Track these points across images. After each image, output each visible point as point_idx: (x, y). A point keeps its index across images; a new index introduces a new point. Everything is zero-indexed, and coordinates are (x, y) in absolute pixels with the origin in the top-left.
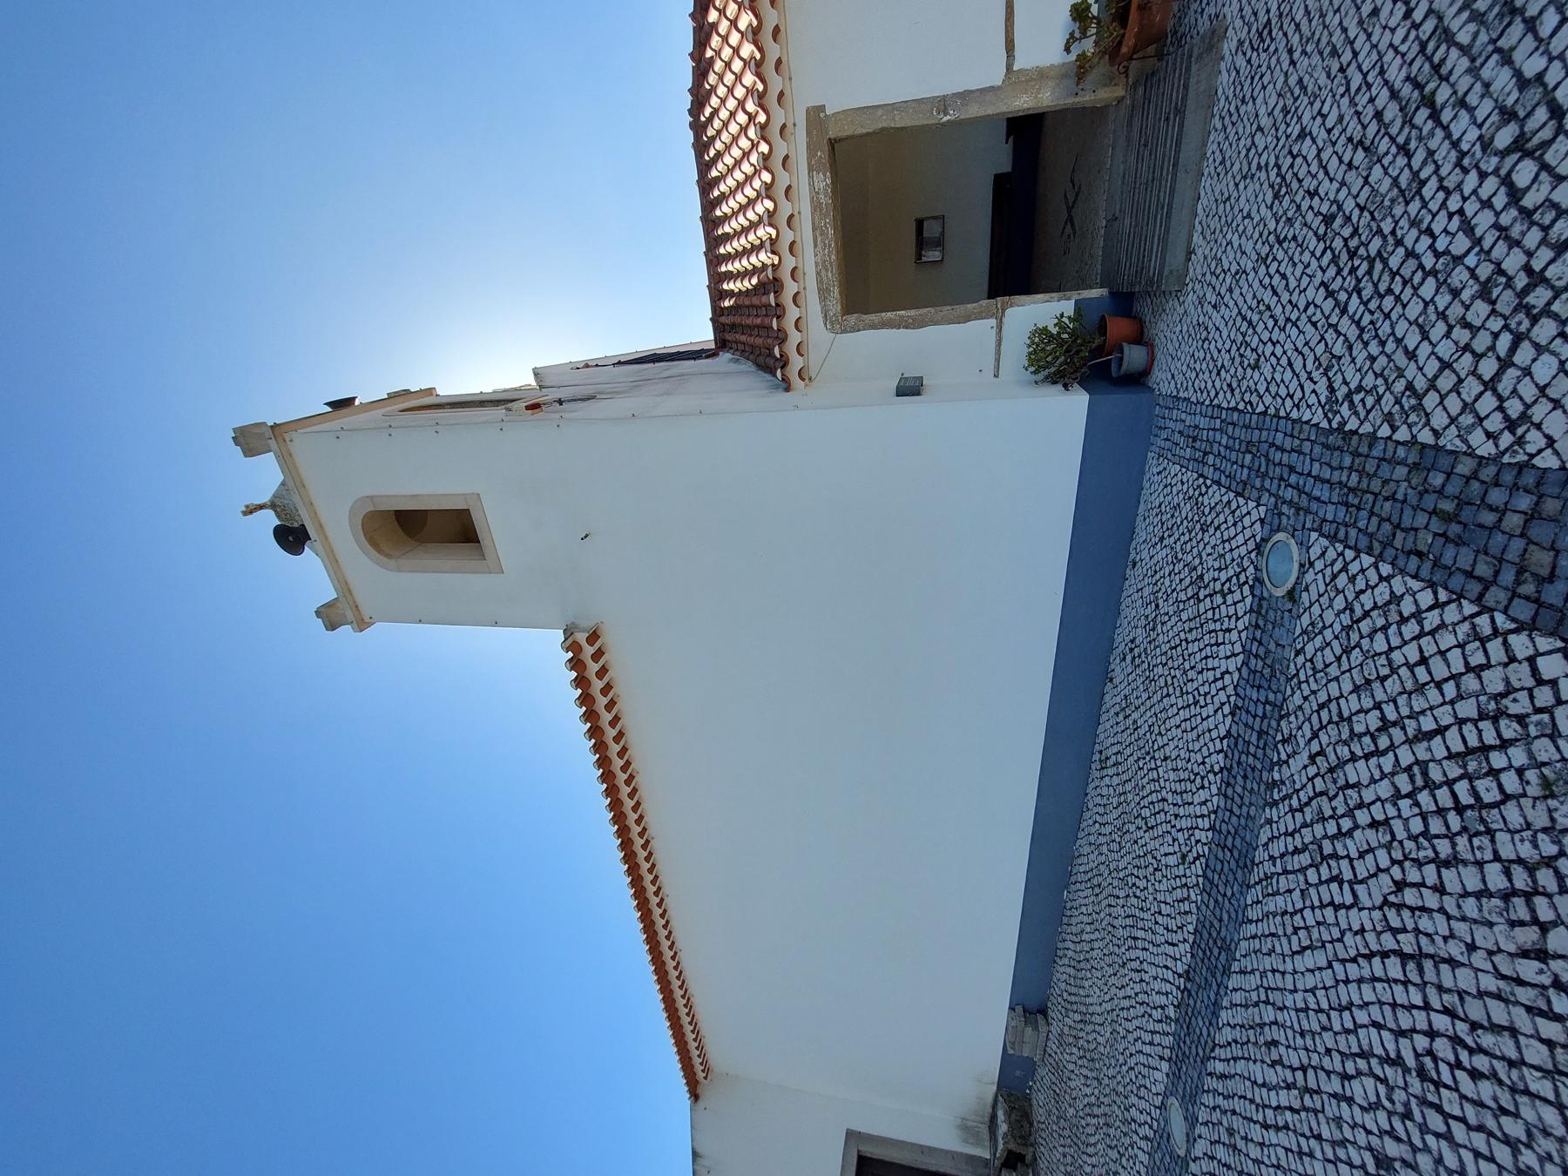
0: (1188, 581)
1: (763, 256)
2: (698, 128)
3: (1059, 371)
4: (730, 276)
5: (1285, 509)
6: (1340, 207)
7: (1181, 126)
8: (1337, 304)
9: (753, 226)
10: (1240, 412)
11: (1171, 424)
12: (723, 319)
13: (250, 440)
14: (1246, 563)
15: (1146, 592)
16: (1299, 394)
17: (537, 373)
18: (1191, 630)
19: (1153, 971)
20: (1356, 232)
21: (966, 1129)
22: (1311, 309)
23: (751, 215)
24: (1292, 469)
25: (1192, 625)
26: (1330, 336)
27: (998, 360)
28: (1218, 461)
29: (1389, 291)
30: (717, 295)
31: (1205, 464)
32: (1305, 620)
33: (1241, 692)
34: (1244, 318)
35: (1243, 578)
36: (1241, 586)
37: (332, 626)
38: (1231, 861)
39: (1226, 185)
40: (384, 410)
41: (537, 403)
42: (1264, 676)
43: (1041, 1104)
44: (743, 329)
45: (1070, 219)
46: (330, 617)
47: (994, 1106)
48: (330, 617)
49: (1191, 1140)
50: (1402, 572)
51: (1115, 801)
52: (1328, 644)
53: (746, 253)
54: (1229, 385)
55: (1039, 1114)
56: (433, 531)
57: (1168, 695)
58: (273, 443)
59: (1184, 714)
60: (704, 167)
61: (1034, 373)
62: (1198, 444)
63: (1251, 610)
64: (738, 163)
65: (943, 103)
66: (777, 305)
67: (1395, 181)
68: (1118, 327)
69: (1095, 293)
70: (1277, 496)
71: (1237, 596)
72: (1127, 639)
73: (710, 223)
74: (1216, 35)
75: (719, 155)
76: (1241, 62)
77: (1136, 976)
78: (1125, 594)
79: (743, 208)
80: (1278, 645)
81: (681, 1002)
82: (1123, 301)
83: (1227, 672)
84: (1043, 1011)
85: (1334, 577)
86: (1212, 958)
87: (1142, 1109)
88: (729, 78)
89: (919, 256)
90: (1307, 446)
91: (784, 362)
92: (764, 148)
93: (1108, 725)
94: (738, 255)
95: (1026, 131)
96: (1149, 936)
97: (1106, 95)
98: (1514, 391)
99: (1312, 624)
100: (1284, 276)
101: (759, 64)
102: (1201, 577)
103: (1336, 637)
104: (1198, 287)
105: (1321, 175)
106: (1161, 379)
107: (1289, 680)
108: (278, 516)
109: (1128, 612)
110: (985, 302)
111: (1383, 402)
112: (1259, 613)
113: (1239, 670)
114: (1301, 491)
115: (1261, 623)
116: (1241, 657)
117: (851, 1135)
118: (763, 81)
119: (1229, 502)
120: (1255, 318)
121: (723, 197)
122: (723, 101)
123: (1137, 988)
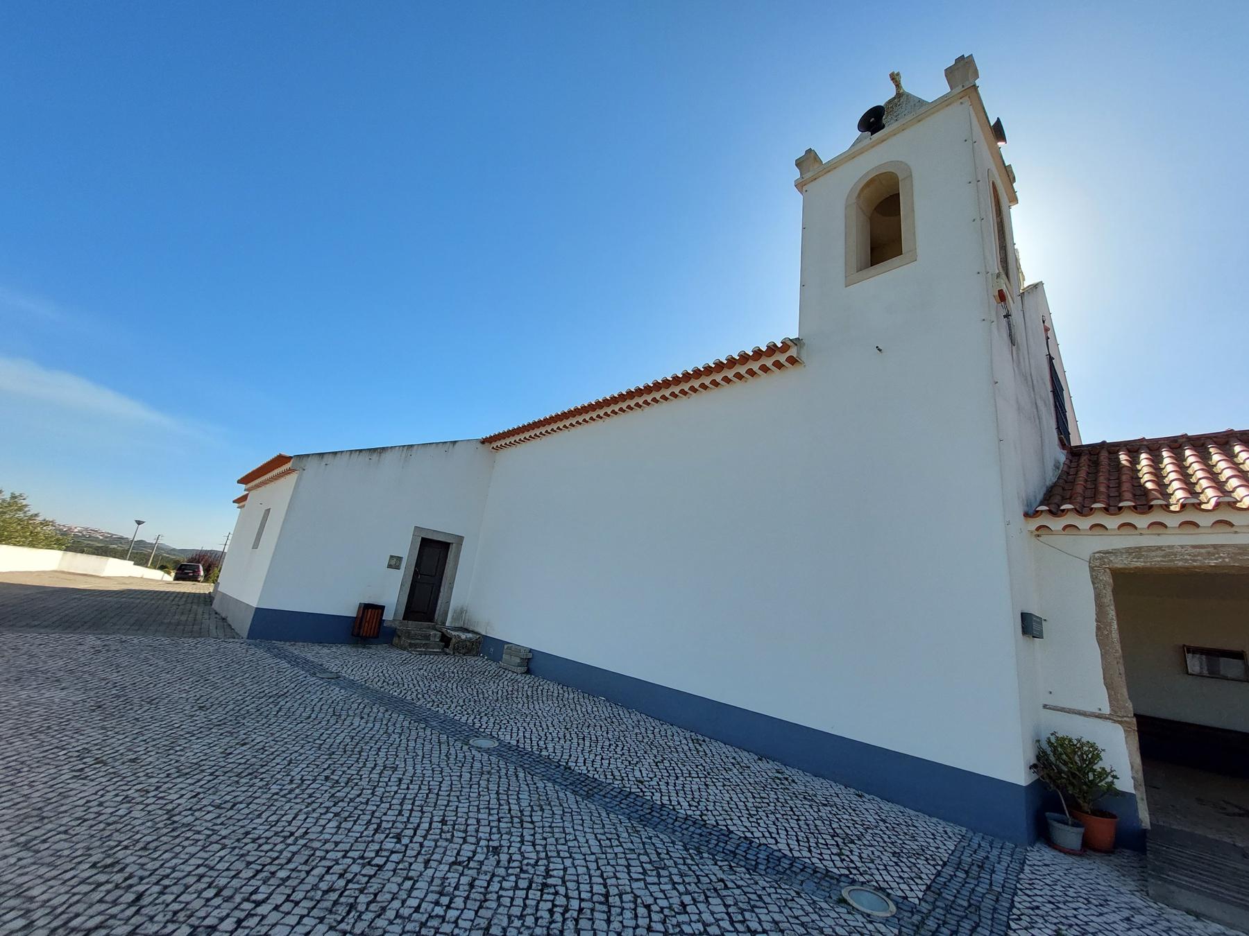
1: (1180, 494)
3: (1051, 764)
4: (1156, 461)
10: (1010, 909)
12: (1104, 454)
13: (962, 73)
14: (867, 877)
15: (836, 799)
17: (1037, 287)
19: (567, 746)
21: (461, 612)
25: (812, 827)
27: (1062, 710)
30: (1134, 448)
32: (824, 905)
33: (763, 848)
35: (854, 871)
36: (848, 868)
37: (799, 163)
38: (649, 815)
41: (1010, 301)
42: (782, 868)
43: (478, 662)
46: (808, 161)
47: (473, 632)
48: (808, 161)
49: (479, 749)
51: (670, 744)
54: (1038, 908)
55: (471, 660)
56: (881, 227)
58: (959, 89)
61: (1049, 742)
63: (828, 871)
66: (1120, 508)
68: (1103, 830)
69: (1144, 816)
71: (839, 864)
77: (561, 735)
81: (537, 432)
84: (528, 672)
86: (586, 787)
87: (488, 724)
91: (1056, 513)
96: (587, 749)
102: (852, 842)
106: (1040, 855)
109: (818, 782)
117: (461, 538)
123: (554, 735)
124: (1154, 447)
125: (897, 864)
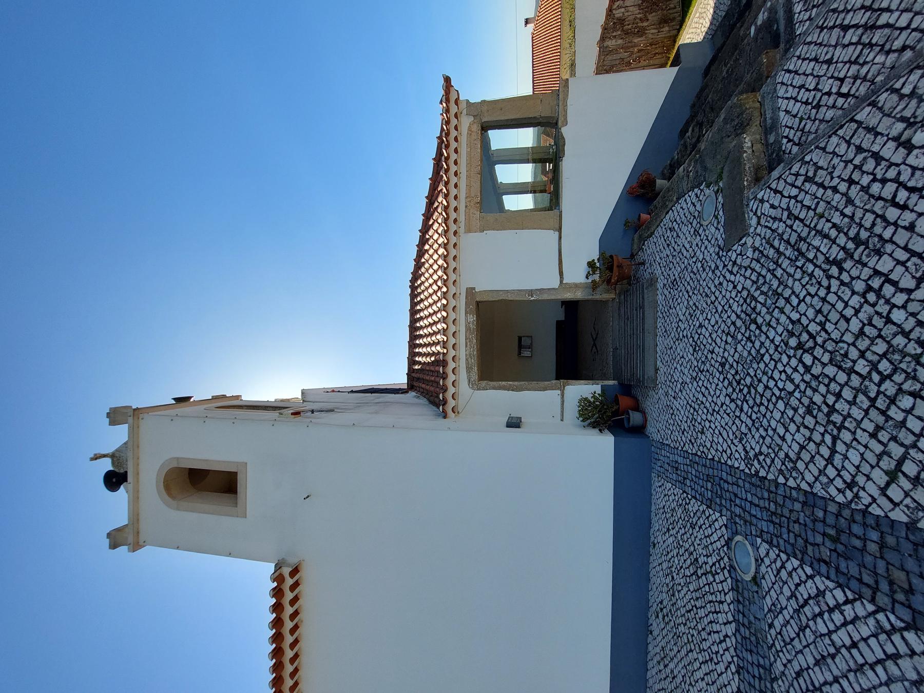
0: (689, 562)
1: (438, 348)
2: (413, 288)
4: (420, 354)
5: (737, 520)
6: (726, 360)
7: (643, 314)
8: (737, 406)
9: (435, 333)
11: (662, 458)
12: (413, 375)
13: (116, 416)
15: (665, 565)
16: (729, 452)
17: (303, 392)
18: (697, 599)
20: (737, 372)
22: (724, 407)
23: (434, 328)
24: (736, 495)
26: (737, 422)
28: (692, 484)
29: (762, 404)
30: (412, 362)
31: (686, 485)
34: (691, 406)
39: (669, 342)
40: (205, 406)
44: (427, 382)
45: (595, 345)
46: (116, 539)
48: (116, 539)
50: (819, 573)
52: (788, 622)
53: (429, 345)
56: (211, 484)
57: (691, 651)
58: (130, 420)
59: (705, 669)
60: (413, 304)
61: (582, 421)
62: (679, 472)
64: (431, 305)
65: (531, 293)
67: (749, 352)
68: (625, 401)
69: (611, 383)
70: (732, 512)
72: (658, 600)
73: (413, 328)
74: (653, 281)
75: (422, 300)
76: (666, 292)
78: (651, 566)
79: (431, 325)
80: (755, 618)
82: (626, 389)
83: (726, 636)
85: (779, 571)
88: (431, 271)
89: (520, 353)
90: (741, 482)
91: (445, 402)
92: (444, 289)
93: (654, 671)
94: (426, 345)
95: (571, 307)
97: (606, 296)
98: (843, 467)
99: (773, 604)
100: (706, 388)
101: (445, 257)
102: (696, 560)
103: (792, 617)
104: (664, 387)
105: (714, 344)
106: (651, 430)
107: (770, 648)
108: (113, 463)
110: (554, 382)
111: (764, 359)
112: (738, 592)
113: (734, 635)
114: (744, 510)
115: (741, 599)
116: (733, 625)
118: (447, 263)
119: (704, 511)
120: (697, 407)
121: (421, 318)
122: (427, 279)
124: (412, 355)
125: (700, 527)
